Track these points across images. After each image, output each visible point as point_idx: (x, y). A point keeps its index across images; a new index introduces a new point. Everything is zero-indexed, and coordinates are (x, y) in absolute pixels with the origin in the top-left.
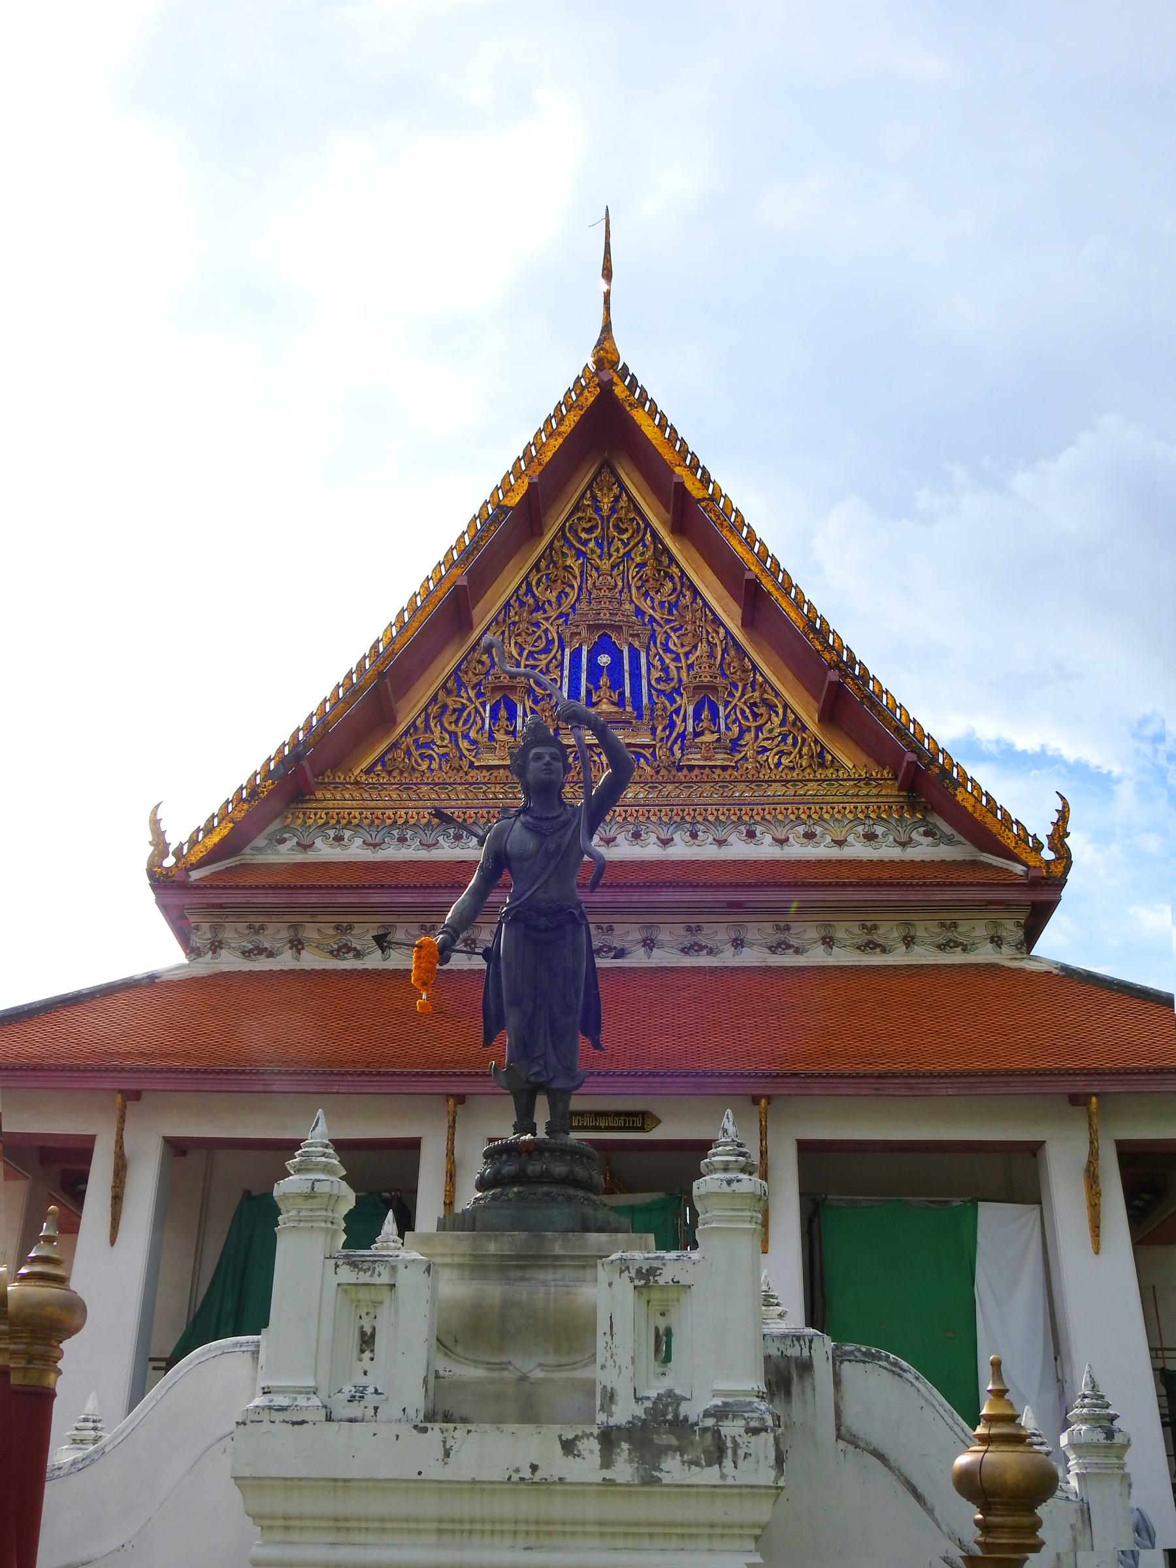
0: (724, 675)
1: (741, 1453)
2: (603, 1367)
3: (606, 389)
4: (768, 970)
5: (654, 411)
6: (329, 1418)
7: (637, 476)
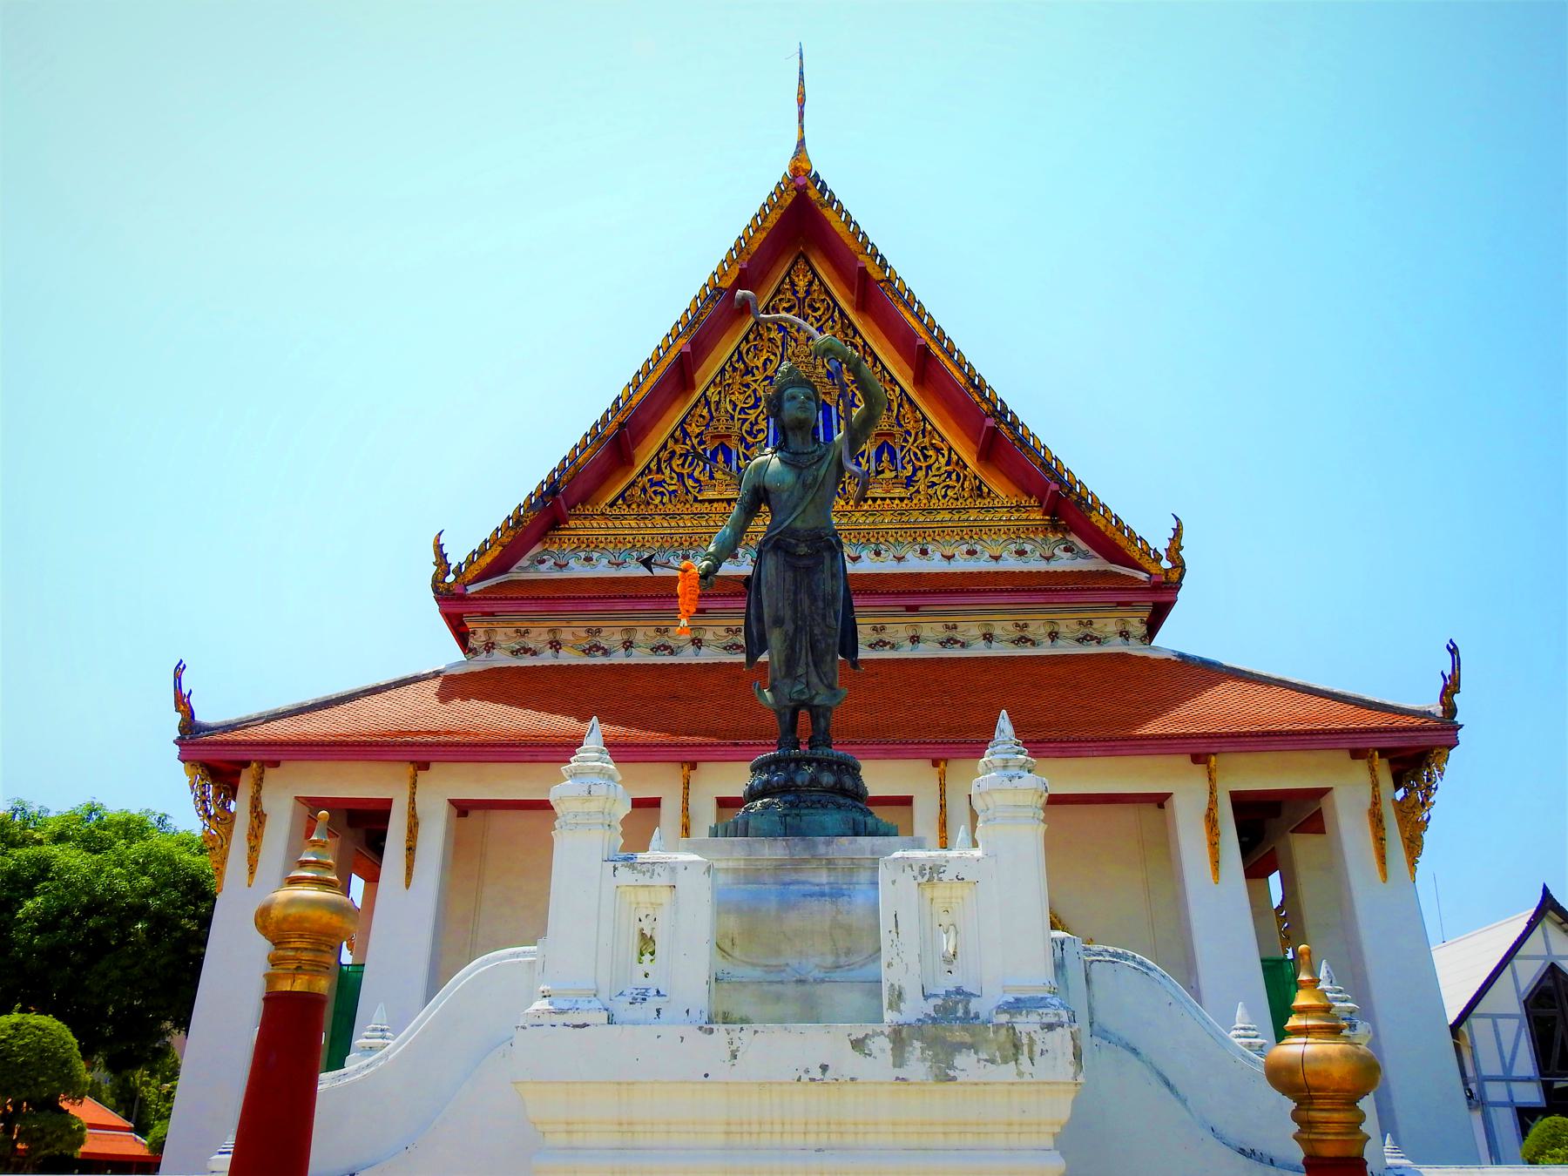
0: (900, 425)
1: (1037, 1049)
2: (890, 965)
3: (801, 193)
5: (841, 210)
6: (610, 1021)
7: (827, 265)
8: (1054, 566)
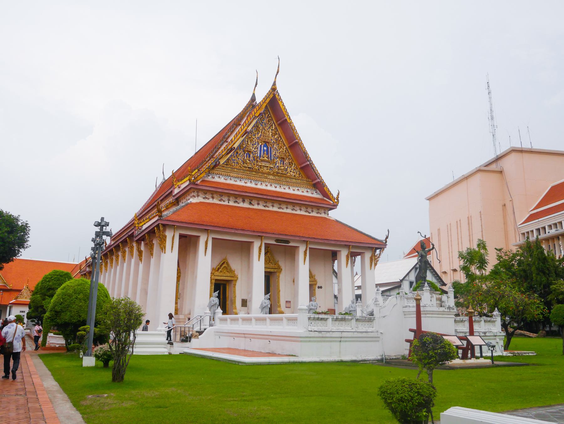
4: (249, 209)
5: (282, 102)
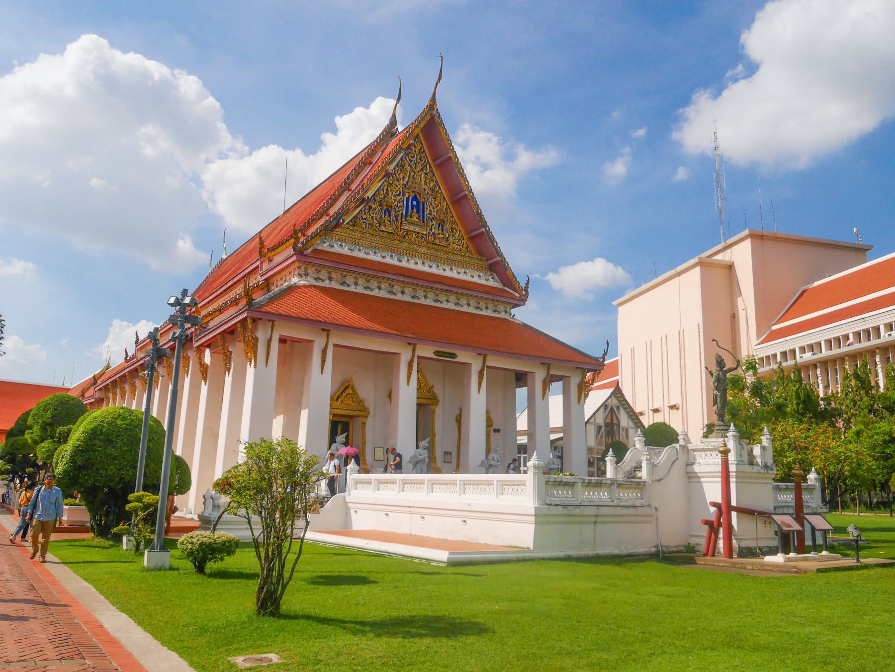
4: (389, 299)
5: (444, 128)
8: (385, 261)
